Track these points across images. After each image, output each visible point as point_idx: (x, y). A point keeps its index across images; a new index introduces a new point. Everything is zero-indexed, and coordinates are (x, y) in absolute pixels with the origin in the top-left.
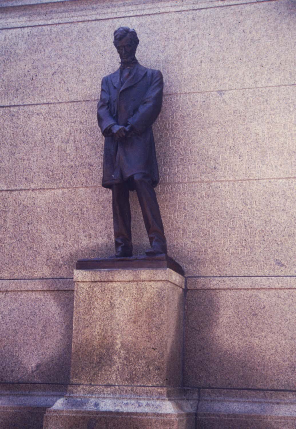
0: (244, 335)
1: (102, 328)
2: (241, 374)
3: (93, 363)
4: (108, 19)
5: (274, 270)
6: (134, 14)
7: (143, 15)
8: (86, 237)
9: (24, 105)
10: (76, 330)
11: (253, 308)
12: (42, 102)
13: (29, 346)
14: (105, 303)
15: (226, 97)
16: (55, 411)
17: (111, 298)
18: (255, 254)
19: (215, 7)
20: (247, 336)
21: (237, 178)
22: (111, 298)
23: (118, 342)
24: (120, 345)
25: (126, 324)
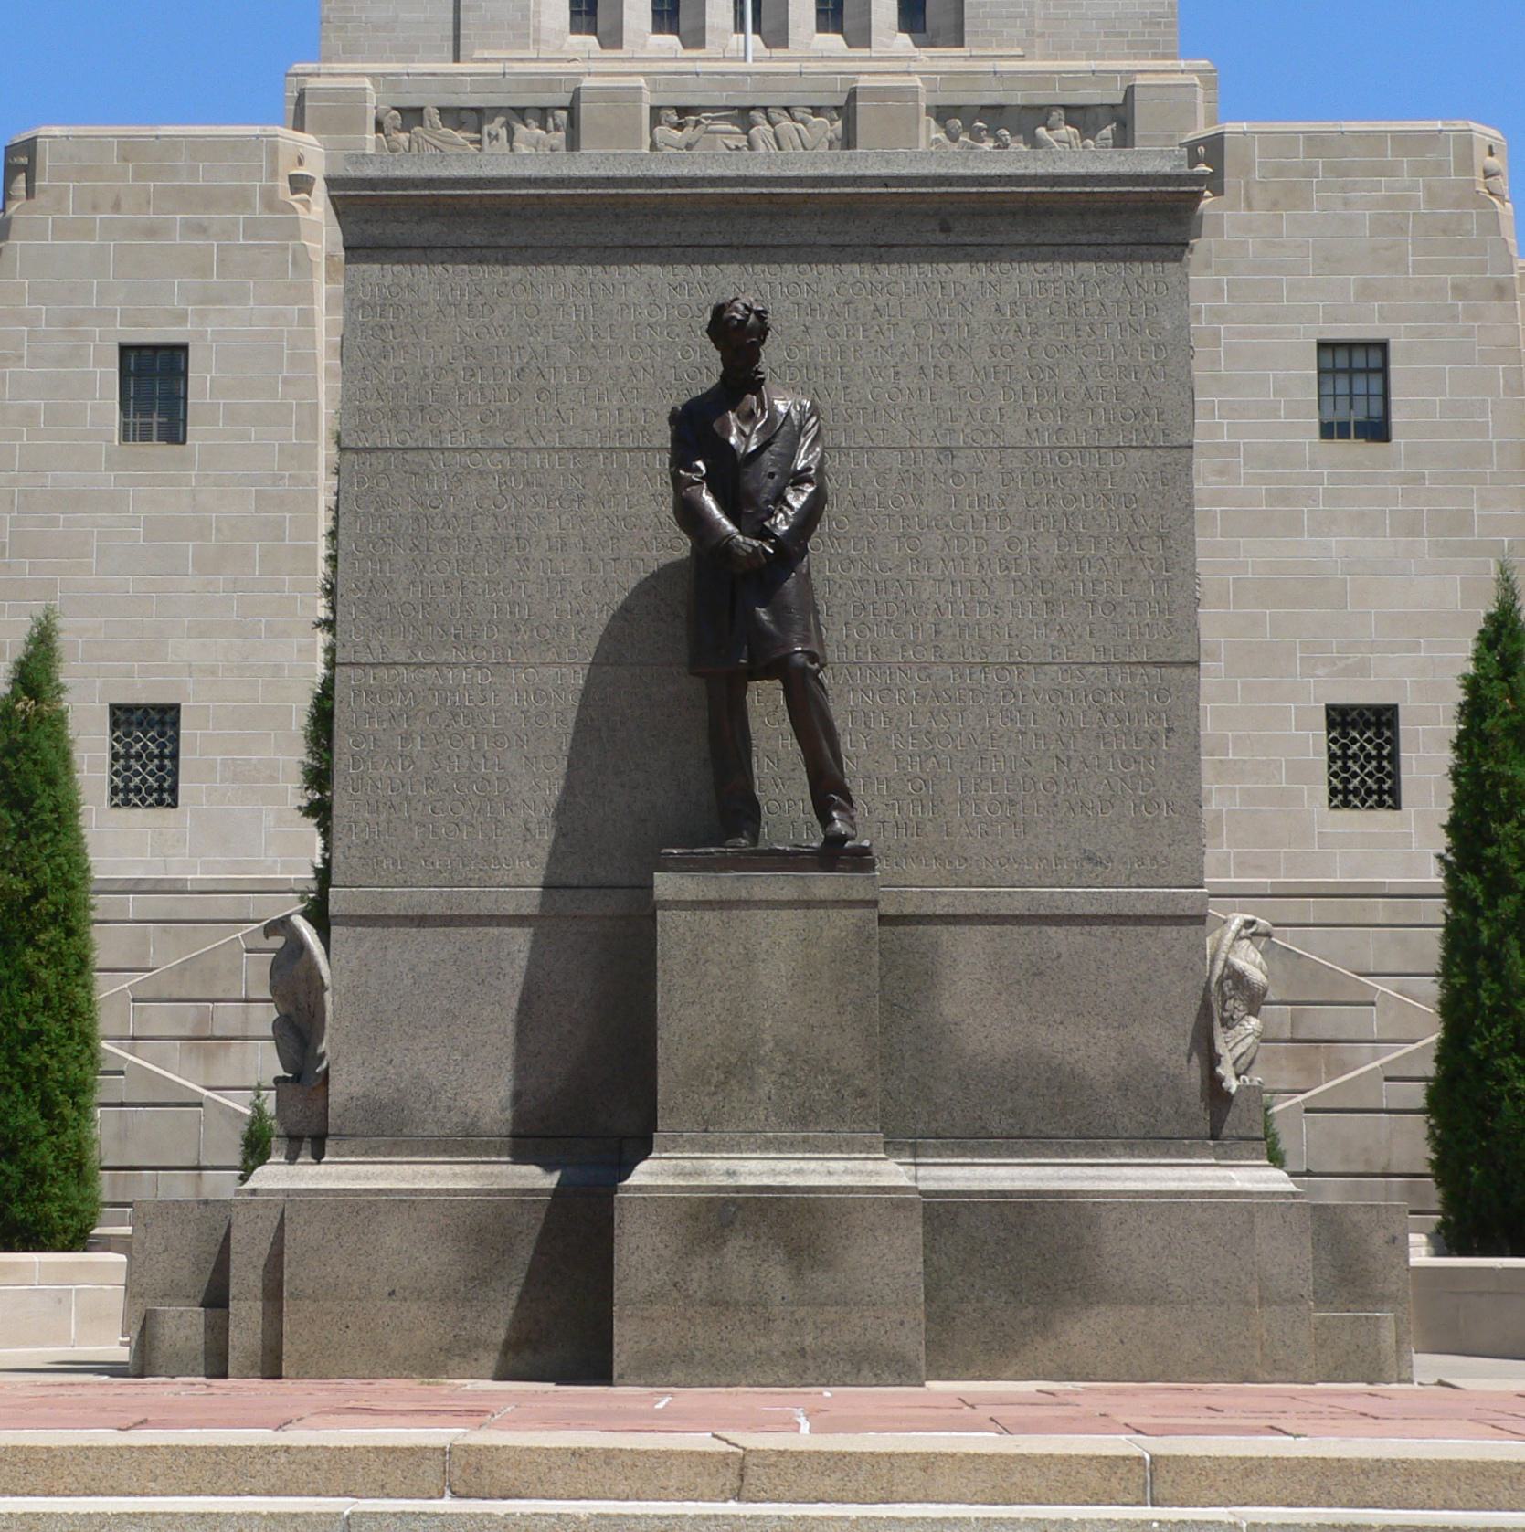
0: (1013, 1019)
1: (728, 1005)
2: (1010, 1105)
3: (709, 1082)
4: (657, 247)
5: (1079, 875)
6: (725, 242)
7: (747, 246)
8: (623, 786)
9: (442, 450)
10: (665, 1009)
11: (1034, 959)
12: (491, 444)
13: (489, 1048)
14: (732, 950)
15: (961, 464)
16: (639, 1188)
17: (747, 938)
18: (1036, 836)
19: (928, 245)
20: (1021, 1021)
21: (991, 659)
22: (747, 938)
23: (767, 1037)
24: (771, 1045)
25: (783, 997)
